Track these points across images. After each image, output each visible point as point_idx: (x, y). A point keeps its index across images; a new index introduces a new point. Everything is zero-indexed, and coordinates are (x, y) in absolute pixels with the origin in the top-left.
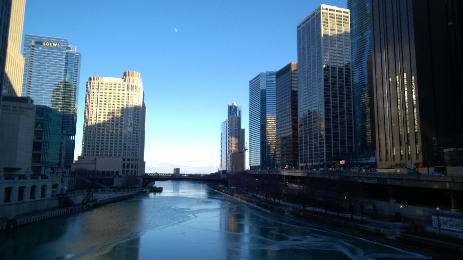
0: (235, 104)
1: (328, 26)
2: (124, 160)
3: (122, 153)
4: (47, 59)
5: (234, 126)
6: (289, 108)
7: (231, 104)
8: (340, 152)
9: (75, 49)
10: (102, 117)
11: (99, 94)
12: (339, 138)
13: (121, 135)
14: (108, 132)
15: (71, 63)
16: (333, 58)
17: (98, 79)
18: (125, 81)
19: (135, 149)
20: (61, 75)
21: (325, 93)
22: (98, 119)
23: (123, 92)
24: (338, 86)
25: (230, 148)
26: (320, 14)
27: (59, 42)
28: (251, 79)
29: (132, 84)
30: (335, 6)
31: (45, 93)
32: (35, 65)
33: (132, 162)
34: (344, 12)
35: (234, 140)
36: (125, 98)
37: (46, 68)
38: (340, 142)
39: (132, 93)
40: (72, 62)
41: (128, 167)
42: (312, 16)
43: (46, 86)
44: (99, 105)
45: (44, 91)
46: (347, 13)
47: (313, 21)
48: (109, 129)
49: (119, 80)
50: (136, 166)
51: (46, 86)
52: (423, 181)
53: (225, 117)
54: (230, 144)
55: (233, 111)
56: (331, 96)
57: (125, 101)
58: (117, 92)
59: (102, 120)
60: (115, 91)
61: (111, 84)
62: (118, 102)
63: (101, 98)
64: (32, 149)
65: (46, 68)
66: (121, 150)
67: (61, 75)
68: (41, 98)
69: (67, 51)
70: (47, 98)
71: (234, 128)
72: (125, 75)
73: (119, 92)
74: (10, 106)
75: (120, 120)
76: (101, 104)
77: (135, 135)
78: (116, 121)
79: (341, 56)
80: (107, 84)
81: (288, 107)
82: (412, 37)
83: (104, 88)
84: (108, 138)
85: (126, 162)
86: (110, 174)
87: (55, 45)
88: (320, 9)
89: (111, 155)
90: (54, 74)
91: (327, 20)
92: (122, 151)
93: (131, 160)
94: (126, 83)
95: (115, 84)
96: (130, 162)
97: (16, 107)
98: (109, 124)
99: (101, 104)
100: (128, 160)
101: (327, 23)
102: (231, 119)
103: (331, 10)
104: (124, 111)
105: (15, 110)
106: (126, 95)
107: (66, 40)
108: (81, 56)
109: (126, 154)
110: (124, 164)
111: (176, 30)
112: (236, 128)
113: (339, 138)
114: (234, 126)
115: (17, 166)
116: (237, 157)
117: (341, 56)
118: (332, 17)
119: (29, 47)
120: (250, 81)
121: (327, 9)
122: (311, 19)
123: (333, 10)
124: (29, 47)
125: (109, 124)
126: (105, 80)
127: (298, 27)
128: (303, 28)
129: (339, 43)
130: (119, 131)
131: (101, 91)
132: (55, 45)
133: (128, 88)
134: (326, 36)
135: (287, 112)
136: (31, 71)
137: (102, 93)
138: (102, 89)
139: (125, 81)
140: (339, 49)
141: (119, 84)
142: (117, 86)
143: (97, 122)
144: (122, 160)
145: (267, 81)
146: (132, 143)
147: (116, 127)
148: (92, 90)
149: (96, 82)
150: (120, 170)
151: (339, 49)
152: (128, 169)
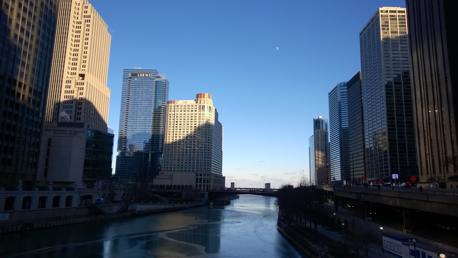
0: (320, 117)
1: (388, 29)
2: (197, 175)
3: (195, 168)
4: (141, 88)
5: (320, 139)
6: (360, 119)
7: (316, 118)
8: (408, 165)
9: (163, 78)
10: (178, 136)
11: (176, 116)
12: (407, 150)
13: (194, 152)
14: (183, 150)
15: (160, 90)
16: (395, 62)
17: (174, 102)
18: (197, 102)
19: (207, 164)
20: (152, 101)
21: (387, 101)
22: (174, 138)
23: (196, 112)
24: (403, 92)
25: (317, 162)
26: (379, 17)
27: (150, 73)
28: (330, 92)
29: (203, 105)
30: (398, 6)
31: (140, 117)
32: (132, 94)
33: (201, 177)
34: (399, 12)
35: (321, 154)
36: (197, 118)
37: (140, 96)
38: (407, 154)
39: (203, 113)
40: (161, 89)
41: (201, 182)
42: (372, 21)
43: (140, 111)
44: (175, 126)
45: (139, 115)
46: (403, 12)
47: (373, 25)
48: (184, 147)
49: (192, 102)
50: (208, 181)
51: (140, 111)
52: (383, 196)
53: (311, 131)
54: (317, 158)
55: (318, 123)
56: (395, 104)
57: (197, 120)
58: (190, 112)
59: (178, 138)
60: (188, 113)
61: (185, 106)
62: (192, 122)
63: (177, 119)
64: (83, 166)
65: (140, 96)
66: (194, 165)
67: (152, 101)
68: (137, 122)
69: (157, 79)
70: (141, 122)
71: (320, 142)
72: (198, 96)
73: (192, 112)
74: (67, 131)
75: (193, 138)
76: (177, 124)
77: (207, 151)
78: (190, 140)
79: (406, 59)
80: (182, 106)
81: (358, 118)
82: (444, 32)
83: (179, 110)
84: (183, 155)
85: (199, 177)
86: (165, 188)
87: (147, 75)
88: (378, 12)
89: (186, 171)
90: (146, 100)
91: (388, 22)
92: (195, 167)
93: (203, 175)
94: (198, 105)
95: (189, 106)
96: (203, 177)
97: (71, 131)
98: (183, 142)
99: (177, 124)
100: (201, 175)
101: (388, 26)
102: (316, 134)
103: (391, 12)
104: (199, 129)
105: (71, 134)
106: (198, 115)
107: (156, 70)
108: (168, 83)
109: (199, 169)
110: (197, 179)
111: (278, 48)
112: (323, 142)
113: (407, 150)
114: (320, 139)
115: (70, 181)
116: (323, 172)
117: (406, 59)
118: (393, 18)
119: (127, 79)
120: (329, 94)
121: (387, 11)
122: (371, 24)
123: (395, 12)
124: (127, 79)
125: (183, 142)
126: (180, 102)
127: (360, 34)
128: (365, 34)
129: (403, 46)
130: (192, 149)
131: (177, 113)
132: (147, 75)
133: (200, 108)
134: (387, 39)
135: (358, 124)
136: (128, 99)
137: (178, 114)
138: (178, 111)
139: (197, 102)
140: (403, 52)
141: (192, 106)
142: (190, 107)
143: (174, 141)
144: (195, 175)
145: (341, 93)
146: (203, 159)
147: (190, 144)
148: (169, 113)
149: (173, 105)
150: (194, 184)
151: (403, 52)
152: (201, 184)
